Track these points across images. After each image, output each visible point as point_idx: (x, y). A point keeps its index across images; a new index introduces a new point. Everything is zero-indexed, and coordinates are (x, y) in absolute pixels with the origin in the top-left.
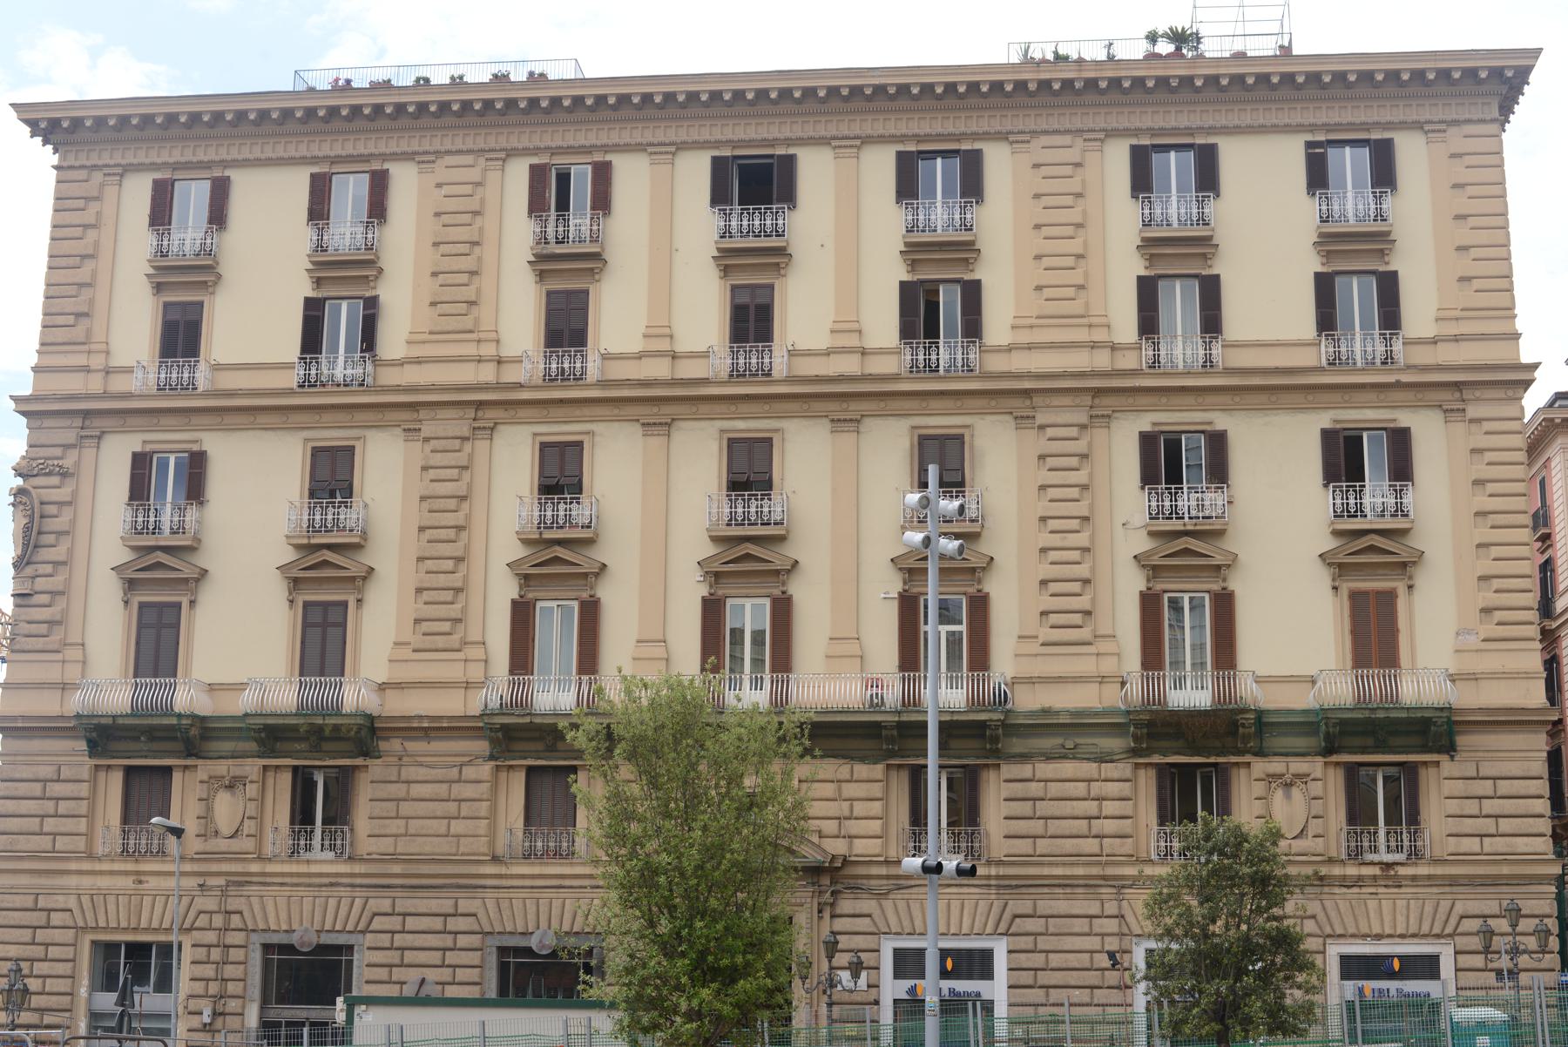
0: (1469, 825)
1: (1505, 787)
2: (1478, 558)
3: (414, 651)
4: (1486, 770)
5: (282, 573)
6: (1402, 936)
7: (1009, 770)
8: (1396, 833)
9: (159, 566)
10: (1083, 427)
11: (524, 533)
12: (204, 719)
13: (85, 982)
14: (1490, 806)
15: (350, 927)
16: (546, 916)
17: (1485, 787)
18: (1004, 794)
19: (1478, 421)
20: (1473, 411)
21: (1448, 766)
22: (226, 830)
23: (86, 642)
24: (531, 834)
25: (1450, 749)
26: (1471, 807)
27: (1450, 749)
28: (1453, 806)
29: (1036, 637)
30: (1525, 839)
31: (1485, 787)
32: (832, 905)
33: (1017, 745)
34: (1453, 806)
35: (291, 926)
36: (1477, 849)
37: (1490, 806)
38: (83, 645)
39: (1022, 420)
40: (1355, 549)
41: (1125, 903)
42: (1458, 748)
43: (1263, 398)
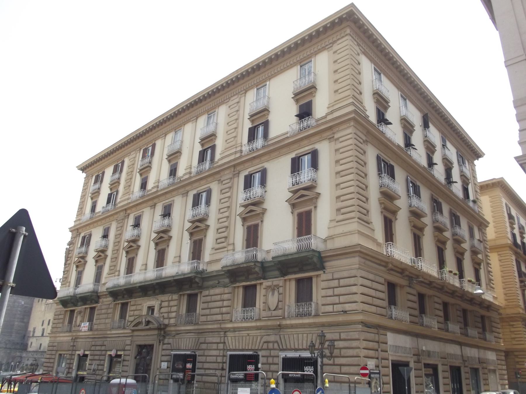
0: (330, 300)
1: (342, 282)
2: (336, 190)
3: (337, 222)
4: (336, 276)
5: (188, 231)
6: (250, 350)
7: (206, 293)
8: (302, 305)
9: (303, 196)
10: (231, 178)
11: (155, 231)
12: (319, 252)
13: (56, 364)
14: (337, 291)
15: (194, 349)
16: (293, 343)
17: (335, 283)
18: (202, 301)
19: (338, 139)
20: (336, 136)
21: (324, 277)
22: (273, 307)
23: (235, 243)
24: (298, 306)
25: (323, 268)
26: (330, 292)
27: (323, 268)
28: (324, 293)
29: (335, 220)
30: (349, 304)
31: (335, 283)
32: (163, 340)
33: (207, 284)
34: (324, 293)
35: (287, 347)
36: (331, 310)
37: (337, 291)
38: (234, 244)
39: (331, 139)
40: (247, 212)
41: (226, 338)
42: (326, 268)
43: (276, 154)
